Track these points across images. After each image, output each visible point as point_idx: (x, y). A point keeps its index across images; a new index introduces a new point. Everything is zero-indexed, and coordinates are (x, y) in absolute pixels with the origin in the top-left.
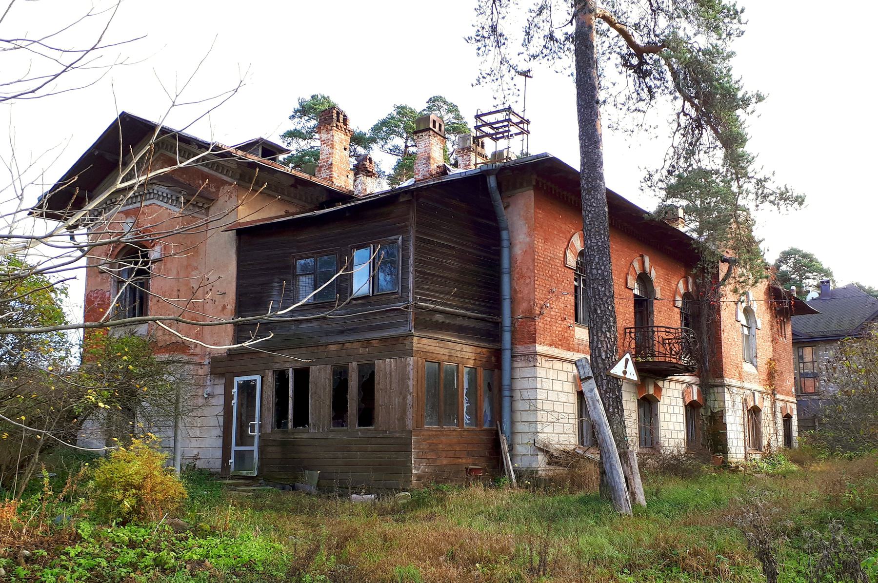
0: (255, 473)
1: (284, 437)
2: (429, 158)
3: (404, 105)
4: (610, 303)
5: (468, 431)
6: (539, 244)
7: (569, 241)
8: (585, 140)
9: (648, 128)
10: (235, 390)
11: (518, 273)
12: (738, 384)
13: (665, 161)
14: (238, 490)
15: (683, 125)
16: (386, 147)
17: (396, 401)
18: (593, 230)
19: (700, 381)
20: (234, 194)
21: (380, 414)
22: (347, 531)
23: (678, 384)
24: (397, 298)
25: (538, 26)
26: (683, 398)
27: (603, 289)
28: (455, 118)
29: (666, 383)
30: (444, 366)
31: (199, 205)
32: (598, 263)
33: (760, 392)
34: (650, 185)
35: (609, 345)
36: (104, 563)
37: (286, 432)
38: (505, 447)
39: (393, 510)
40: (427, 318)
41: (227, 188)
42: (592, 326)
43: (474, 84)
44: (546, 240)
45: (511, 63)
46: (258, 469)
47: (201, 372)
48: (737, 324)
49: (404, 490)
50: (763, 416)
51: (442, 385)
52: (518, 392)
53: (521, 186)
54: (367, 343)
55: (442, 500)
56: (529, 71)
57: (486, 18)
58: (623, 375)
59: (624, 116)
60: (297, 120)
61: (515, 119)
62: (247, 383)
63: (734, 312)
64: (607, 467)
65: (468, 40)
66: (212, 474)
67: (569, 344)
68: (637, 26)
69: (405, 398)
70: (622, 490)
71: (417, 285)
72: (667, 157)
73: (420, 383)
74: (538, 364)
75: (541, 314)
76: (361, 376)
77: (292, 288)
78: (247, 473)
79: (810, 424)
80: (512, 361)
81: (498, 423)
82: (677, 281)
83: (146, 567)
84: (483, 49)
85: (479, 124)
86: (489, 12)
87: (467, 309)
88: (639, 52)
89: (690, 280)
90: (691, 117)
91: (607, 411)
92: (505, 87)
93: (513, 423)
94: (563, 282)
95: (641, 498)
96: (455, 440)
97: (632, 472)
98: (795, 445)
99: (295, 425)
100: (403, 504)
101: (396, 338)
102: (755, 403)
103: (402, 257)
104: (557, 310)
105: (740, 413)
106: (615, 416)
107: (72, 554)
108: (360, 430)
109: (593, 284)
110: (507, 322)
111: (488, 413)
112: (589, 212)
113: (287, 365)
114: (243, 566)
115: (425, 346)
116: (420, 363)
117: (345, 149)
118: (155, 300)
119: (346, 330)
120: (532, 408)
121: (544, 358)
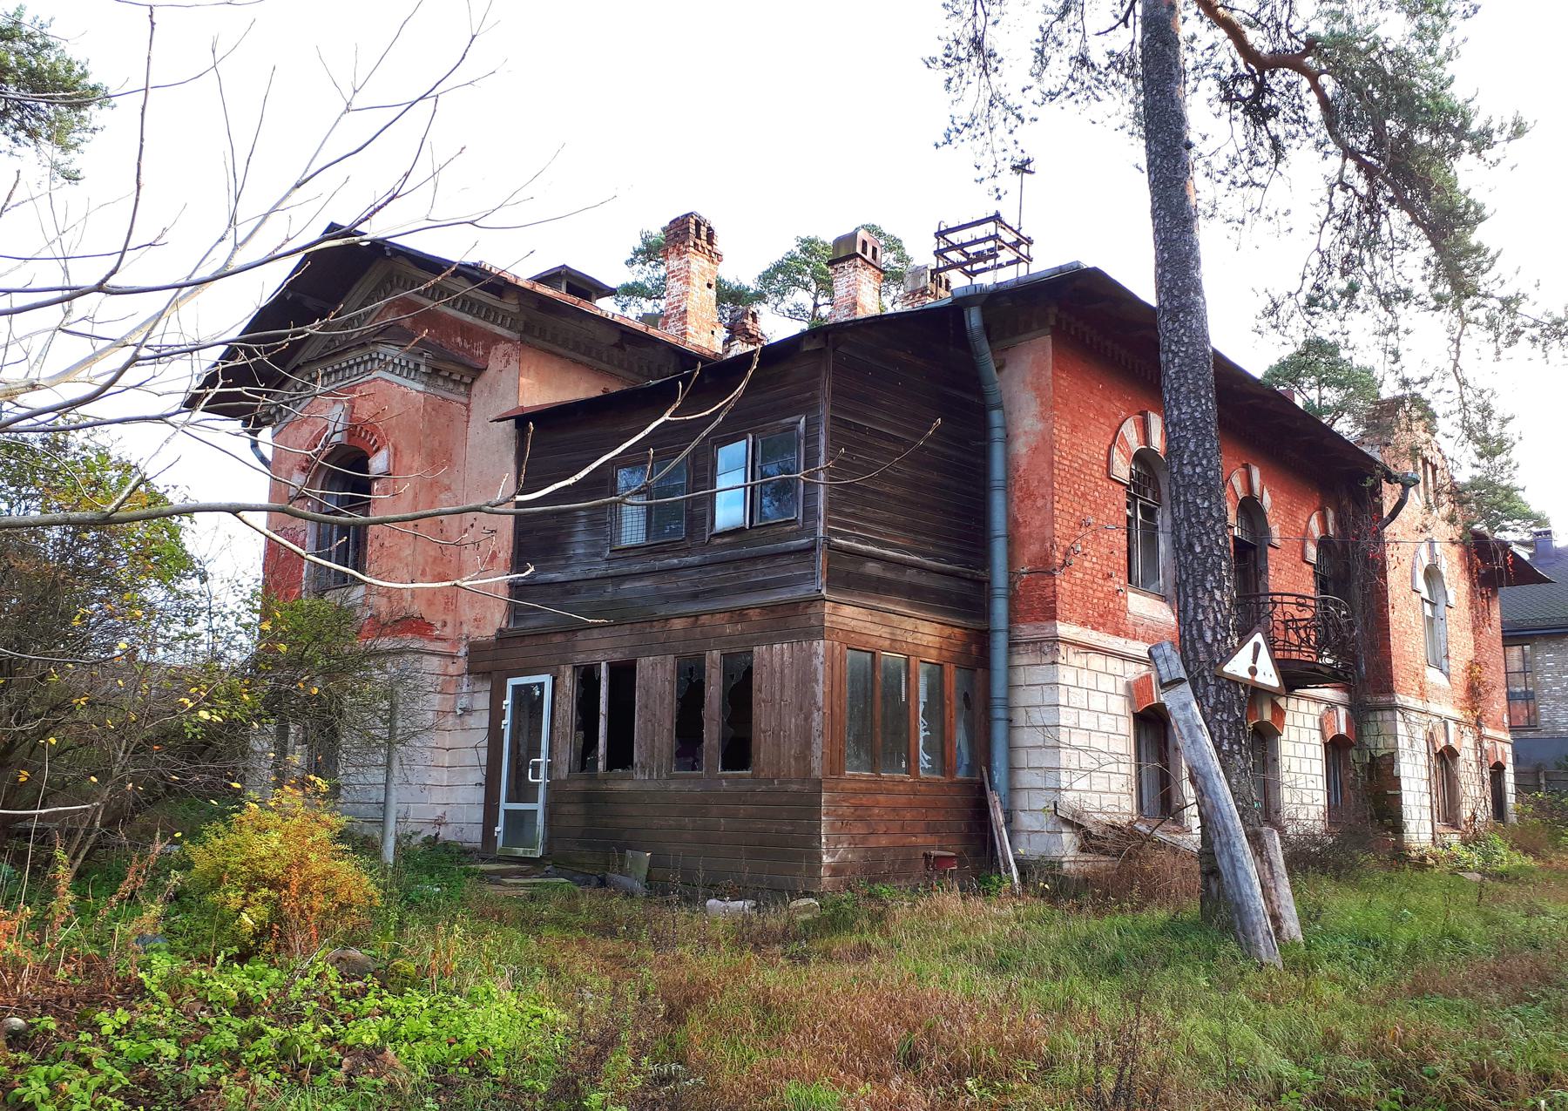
0: (539, 853)
1: (591, 786)
2: (855, 304)
3: (812, 237)
4: (1220, 532)
5: (928, 783)
6: (1062, 434)
7: (1117, 432)
8: (1164, 217)
9: (1272, 215)
10: (508, 701)
11: (1021, 489)
12: (1419, 705)
13: (1304, 278)
14: (505, 885)
15: (1339, 209)
16: (782, 306)
17: (792, 722)
18: (1183, 389)
19: (1350, 699)
20: (515, 357)
21: (763, 750)
22: (691, 982)
23: (1312, 705)
24: (796, 531)
25: (1060, 38)
26: (1322, 730)
27: (1206, 504)
28: (898, 261)
29: (1292, 701)
30: (883, 659)
31: (454, 377)
32: (1195, 453)
33: (1457, 722)
34: (1274, 323)
35: (1219, 616)
36: (171, 1050)
37: (593, 778)
38: (998, 816)
39: (785, 934)
40: (851, 568)
41: (503, 347)
42: (1184, 577)
43: (940, 144)
44: (1074, 428)
45: (1009, 102)
46: (544, 844)
47: (452, 670)
48: (1415, 597)
49: (807, 894)
50: (1462, 766)
51: (878, 694)
52: (1022, 712)
53: (1028, 328)
54: (740, 614)
55: (880, 916)
56: (1028, 161)
57: (963, 22)
58: (1249, 677)
59: (1226, 192)
60: (638, 267)
61: (1009, 237)
62: (528, 687)
63: (1408, 574)
64: (1224, 863)
65: (930, 62)
66: (466, 852)
67: (1117, 623)
68: (1256, 22)
69: (808, 718)
70: (1257, 912)
71: (832, 507)
72: (1308, 271)
73: (836, 689)
74: (1060, 660)
75: (1064, 564)
76: (727, 674)
77: (609, 519)
78: (525, 852)
79: (1529, 782)
80: (1010, 654)
81: (984, 769)
82: (1307, 515)
83: (259, 1060)
84: (956, 80)
85: (942, 246)
86: (968, 12)
87: (924, 554)
88: (1261, 64)
89: (1331, 515)
90: (1356, 194)
91: (1218, 748)
92: (998, 146)
93: (1012, 769)
94: (1106, 506)
95: (1292, 926)
96: (903, 799)
97: (1272, 874)
98: (1512, 818)
99: (610, 766)
100: (805, 923)
101: (794, 605)
102: (1447, 740)
103: (806, 455)
104: (1094, 560)
105: (1422, 759)
106: (1233, 757)
107: (107, 1029)
108: (726, 778)
109: (1185, 495)
110: (1000, 578)
111: (965, 751)
112: (1176, 354)
113: (598, 657)
114: (463, 1062)
115: (847, 621)
116: (837, 652)
117: (709, 286)
118: (376, 545)
119: (704, 592)
120: (1050, 743)
121: (1071, 649)
